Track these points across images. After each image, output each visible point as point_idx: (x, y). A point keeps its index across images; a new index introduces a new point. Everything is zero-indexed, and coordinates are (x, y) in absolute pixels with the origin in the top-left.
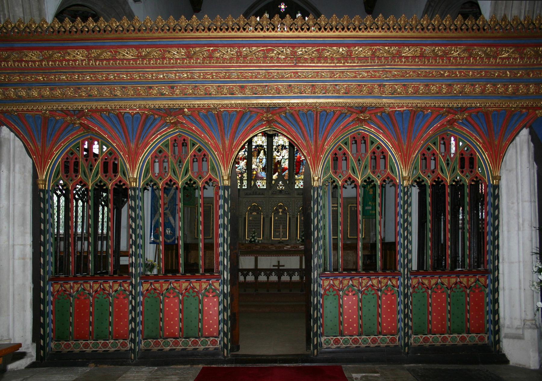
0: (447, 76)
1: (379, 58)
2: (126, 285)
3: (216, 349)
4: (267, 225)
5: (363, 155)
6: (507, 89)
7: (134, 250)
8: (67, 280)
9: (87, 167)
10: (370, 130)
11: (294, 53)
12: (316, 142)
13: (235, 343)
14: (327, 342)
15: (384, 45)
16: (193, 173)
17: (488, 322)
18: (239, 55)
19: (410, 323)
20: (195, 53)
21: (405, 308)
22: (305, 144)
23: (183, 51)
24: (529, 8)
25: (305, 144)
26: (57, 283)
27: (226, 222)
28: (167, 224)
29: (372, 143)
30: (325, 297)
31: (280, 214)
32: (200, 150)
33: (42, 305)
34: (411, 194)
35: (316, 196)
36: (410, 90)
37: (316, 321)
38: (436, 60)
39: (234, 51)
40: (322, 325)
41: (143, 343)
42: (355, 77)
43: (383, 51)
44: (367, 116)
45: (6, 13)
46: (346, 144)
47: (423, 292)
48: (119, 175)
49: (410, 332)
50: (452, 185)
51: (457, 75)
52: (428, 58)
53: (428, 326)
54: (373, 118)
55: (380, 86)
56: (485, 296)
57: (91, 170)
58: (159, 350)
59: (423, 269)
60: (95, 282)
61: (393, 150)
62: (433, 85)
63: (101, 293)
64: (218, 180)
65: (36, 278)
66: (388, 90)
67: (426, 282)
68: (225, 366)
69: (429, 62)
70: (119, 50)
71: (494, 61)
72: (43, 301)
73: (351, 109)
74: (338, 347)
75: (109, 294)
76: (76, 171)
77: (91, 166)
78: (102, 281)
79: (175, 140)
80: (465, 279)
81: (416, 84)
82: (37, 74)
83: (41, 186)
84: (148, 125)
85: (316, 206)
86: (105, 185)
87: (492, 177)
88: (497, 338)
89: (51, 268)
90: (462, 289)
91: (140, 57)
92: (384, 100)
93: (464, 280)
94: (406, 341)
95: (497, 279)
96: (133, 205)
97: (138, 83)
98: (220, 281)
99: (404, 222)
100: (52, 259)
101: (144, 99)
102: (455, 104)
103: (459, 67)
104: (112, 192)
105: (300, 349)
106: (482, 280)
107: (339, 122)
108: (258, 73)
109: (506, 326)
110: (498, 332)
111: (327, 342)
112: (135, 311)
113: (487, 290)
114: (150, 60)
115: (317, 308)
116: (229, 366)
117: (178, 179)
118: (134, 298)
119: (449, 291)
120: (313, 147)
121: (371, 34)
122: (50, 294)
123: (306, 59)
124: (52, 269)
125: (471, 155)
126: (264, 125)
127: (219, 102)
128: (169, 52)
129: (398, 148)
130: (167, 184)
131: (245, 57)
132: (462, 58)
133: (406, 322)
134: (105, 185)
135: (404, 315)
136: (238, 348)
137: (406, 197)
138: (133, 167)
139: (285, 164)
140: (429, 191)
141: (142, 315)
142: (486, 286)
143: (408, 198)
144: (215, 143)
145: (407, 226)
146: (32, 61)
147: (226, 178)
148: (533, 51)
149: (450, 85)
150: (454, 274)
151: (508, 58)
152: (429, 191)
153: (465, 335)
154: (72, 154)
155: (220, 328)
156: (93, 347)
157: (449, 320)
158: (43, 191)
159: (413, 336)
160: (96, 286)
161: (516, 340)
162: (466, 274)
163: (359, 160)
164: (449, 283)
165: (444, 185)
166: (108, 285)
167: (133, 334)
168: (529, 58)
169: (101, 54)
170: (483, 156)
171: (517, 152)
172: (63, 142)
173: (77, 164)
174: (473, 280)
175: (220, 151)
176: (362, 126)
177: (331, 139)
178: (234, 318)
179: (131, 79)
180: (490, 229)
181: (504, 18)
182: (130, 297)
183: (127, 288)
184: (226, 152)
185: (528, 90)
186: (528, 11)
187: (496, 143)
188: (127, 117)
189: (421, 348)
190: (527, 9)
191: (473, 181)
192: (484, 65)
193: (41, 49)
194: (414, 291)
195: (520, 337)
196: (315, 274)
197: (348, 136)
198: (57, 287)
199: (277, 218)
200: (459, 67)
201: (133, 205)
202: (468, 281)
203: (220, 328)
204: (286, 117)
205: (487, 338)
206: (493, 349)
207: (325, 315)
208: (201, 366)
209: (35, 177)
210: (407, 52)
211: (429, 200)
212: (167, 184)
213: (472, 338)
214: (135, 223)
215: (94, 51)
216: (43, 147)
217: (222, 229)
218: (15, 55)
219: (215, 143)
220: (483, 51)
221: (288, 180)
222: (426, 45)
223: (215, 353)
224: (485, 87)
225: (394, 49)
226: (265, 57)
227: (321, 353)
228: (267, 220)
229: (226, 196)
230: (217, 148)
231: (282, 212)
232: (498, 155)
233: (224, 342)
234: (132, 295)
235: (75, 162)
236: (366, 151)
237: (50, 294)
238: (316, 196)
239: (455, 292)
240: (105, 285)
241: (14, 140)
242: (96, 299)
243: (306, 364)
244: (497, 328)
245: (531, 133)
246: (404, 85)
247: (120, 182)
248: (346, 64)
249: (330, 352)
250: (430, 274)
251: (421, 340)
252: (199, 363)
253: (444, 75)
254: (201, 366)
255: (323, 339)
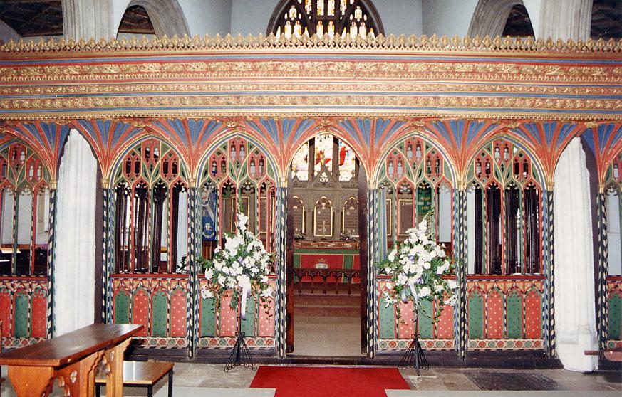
0: (499, 91)
1: (434, 73)
2: (183, 283)
3: (271, 349)
4: (309, 220)
5: (418, 159)
6: (555, 104)
7: (192, 249)
8: (126, 277)
9: (148, 167)
10: (425, 136)
11: (353, 68)
12: (372, 147)
13: (291, 347)
14: (383, 345)
15: (439, 62)
16: (250, 174)
17: (544, 328)
18: (302, 69)
19: (466, 328)
20: (260, 67)
21: (461, 322)
22: (361, 148)
23: (249, 65)
24: (575, 24)
25: (361, 148)
26: (117, 279)
27: (283, 223)
28: (206, 219)
29: (427, 147)
30: (381, 299)
31: (324, 208)
32: (257, 152)
33: (103, 301)
34: (466, 198)
35: (372, 199)
36: (464, 103)
37: (372, 323)
38: (487, 75)
39: (297, 65)
40: (377, 327)
41: (199, 340)
42: (412, 90)
43: (436, 67)
44: (422, 123)
45: (81, 25)
46: (401, 148)
47: (480, 296)
48: (179, 174)
49: (466, 336)
50: (507, 190)
51: (508, 90)
52: (480, 74)
53: (484, 330)
54: (428, 124)
55: (435, 98)
56: (541, 300)
57: (151, 170)
58: (216, 348)
59: (480, 273)
60: (154, 279)
61: (447, 155)
62: (486, 98)
63: (160, 290)
64: (275, 181)
65: (99, 274)
66: (443, 102)
67: (482, 286)
68: (282, 365)
69: (481, 77)
70: (189, 64)
71: (542, 78)
72: (104, 297)
73: (407, 118)
74: (394, 350)
75: (167, 292)
76: (137, 171)
77: (152, 166)
78: (161, 279)
79: (233, 142)
80: (521, 284)
81: (470, 97)
82: (115, 85)
83: (104, 186)
84: (210, 129)
85: (372, 209)
86: (164, 184)
87: (546, 183)
88: (552, 344)
89: (112, 265)
90: (518, 294)
91: (209, 70)
92: (440, 112)
93: (520, 286)
94: (463, 345)
95: (552, 285)
96: (193, 205)
97: (206, 93)
98: (276, 281)
99: (460, 226)
100: (113, 256)
101: (211, 108)
102: (507, 115)
103: (509, 83)
104: (171, 191)
105: (356, 351)
106: (538, 285)
107: (396, 129)
108: (320, 85)
109: (561, 331)
110: (553, 337)
111: (383, 345)
112: (193, 309)
113: (543, 295)
114: (218, 72)
115: (373, 311)
116: (285, 365)
117: (236, 180)
118: (192, 296)
119: (505, 296)
120: (369, 151)
121: (426, 51)
122: (110, 290)
123: (364, 73)
124: (113, 265)
125: (526, 161)
126: (321, 129)
127: (281, 111)
128: (237, 66)
129: (453, 154)
130: (225, 184)
131: (307, 71)
132: (513, 75)
133: (462, 326)
134: (164, 184)
135: (461, 319)
136: (293, 350)
137: (461, 201)
138: (193, 168)
139: (329, 154)
140: (484, 195)
141: (199, 313)
142: (542, 292)
143: (463, 202)
144: (274, 147)
145: (463, 231)
146: (110, 74)
147: (283, 180)
148: (577, 70)
149: (501, 99)
150: (509, 279)
151: (555, 76)
152: (484, 195)
153: (521, 340)
154: (133, 154)
155: (276, 328)
156: (152, 344)
157: (506, 325)
158: (106, 190)
159: (470, 341)
160: (155, 284)
161: (570, 346)
162: (523, 279)
163: (414, 164)
164: (505, 288)
165: (499, 190)
166: (166, 282)
167: (191, 332)
168: (574, 76)
169: (174, 67)
170: (537, 163)
171: (569, 159)
172: (126, 144)
173: (138, 164)
174: (529, 285)
175: (278, 154)
176: (417, 132)
177: (387, 144)
178: (289, 318)
179: (200, 90)
180: (545, 234)
181: (549, 40)
182: (188, 294)
183: (185, 286)
184: (284, 155)
185: (575, 106)
186: (574, 27)
187: (549, 150)
188: (192, 122)
189: (476, 353)
190: (573, 26)
191: (528, 186)
192: (532, 82)
193: (119, 63)
194: (470, 296)
195: (573, 343)
196: (370, 277)
197: (403, 140)
198: (117, 283)
199: (319, 213)
200: (509, 83)
201: (193, 205)
202: (524, 286)
203: (276, 328)
204: (343, 123)
205: (543, 345)
206: (548, 354)
207: (380, 318)
208: (258, 365)
209: (99, 176)
210: (459, 67)
211: (484, 204)
212: (225, 184)
213: (528, 344)
214: (194, 222)
215: (167, 64)
216: (109, 149)
217: (279, 230)
218: (96, 69)
219: (274, 147)
220: (531, 69)
221: (332, 171)
222: (478, 62)
223: (272, 353)
224: (535, 101)
225: (448, 66)
226: (326, 71)
227: (377, 355)
228: (309, 215)
229: (283, 197)
230: (275, 151)
231: (325, 206)
232: (551, 162)
233: (280, 342)
234: (190, 293)
235: (136, 163)
236: (422, 155)
237: (110, 290)
238: (372, 199)
239: (511, 297)
240: (144, 282)
241: (82, 142)
242: (154, 297)
243: (361, 366)
244: (552, 333)
245: (582, 142)
246: (458, 98)
247: (179, 182)
248: (403, 78)
249: (385, 355)
250: (485, 278)
251: (478, 345)
252: (256, 361)
253: (495, 89)
254: (258, 365)
255: (379, 341)
